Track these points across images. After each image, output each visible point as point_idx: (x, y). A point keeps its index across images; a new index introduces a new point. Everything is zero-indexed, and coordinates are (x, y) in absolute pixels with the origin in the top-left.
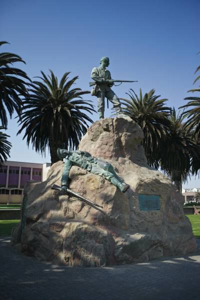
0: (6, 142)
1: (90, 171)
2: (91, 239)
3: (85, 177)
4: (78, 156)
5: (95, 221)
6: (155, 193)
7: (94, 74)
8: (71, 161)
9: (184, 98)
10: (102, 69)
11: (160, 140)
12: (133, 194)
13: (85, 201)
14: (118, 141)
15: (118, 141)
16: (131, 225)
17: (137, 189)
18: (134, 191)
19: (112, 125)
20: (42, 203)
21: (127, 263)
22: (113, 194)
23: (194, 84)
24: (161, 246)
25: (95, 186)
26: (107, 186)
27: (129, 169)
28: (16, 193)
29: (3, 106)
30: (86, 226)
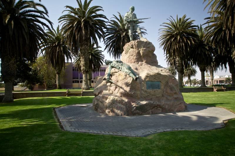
0: (101, 55)
1: (121, 70)
2: (119, 103)
3: (117, 74)
4: (115, 63)
5: (122, 95)
6: (157, 80)
7: (126, 17)
9: (205, 18)
10: (131, 14)
11: (190, 47)
12: (143, 81)
14: (139, 53)
15: (139, 53)
16: (141, 97)
17: (145, 79)
18: (143, 80)
19: (135, 44)
20: (101, 87)
21: (139, 115)
22: (131, 82)
23: (204, 10)
24: (160, 107)
26: (128, 78)
27: (144, 68)
28: (76, 82)
29: (95, 36)
30: (117, 97)
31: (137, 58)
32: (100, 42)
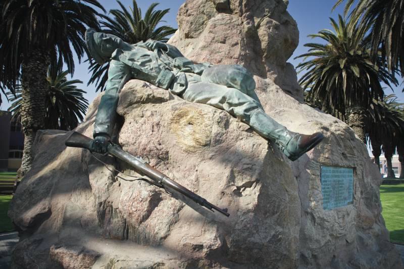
0: (83, 99)
1: (180, 95)
3: (166, 107)
4: (149, 52)
8: (126, 66)
13: (162, 185)
14: (252, 36)
25: (197, 136)
31: (246, 54)
32: (80, 63)
